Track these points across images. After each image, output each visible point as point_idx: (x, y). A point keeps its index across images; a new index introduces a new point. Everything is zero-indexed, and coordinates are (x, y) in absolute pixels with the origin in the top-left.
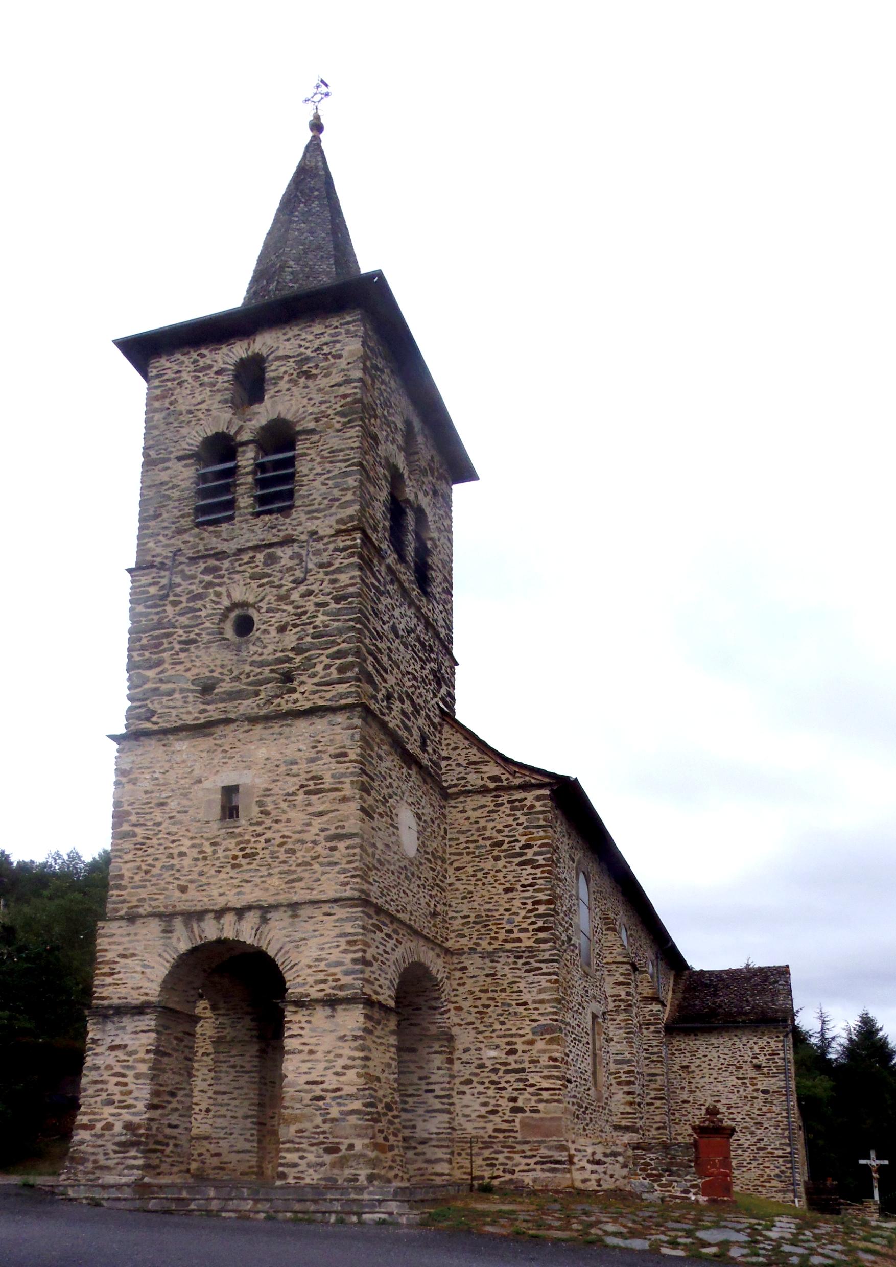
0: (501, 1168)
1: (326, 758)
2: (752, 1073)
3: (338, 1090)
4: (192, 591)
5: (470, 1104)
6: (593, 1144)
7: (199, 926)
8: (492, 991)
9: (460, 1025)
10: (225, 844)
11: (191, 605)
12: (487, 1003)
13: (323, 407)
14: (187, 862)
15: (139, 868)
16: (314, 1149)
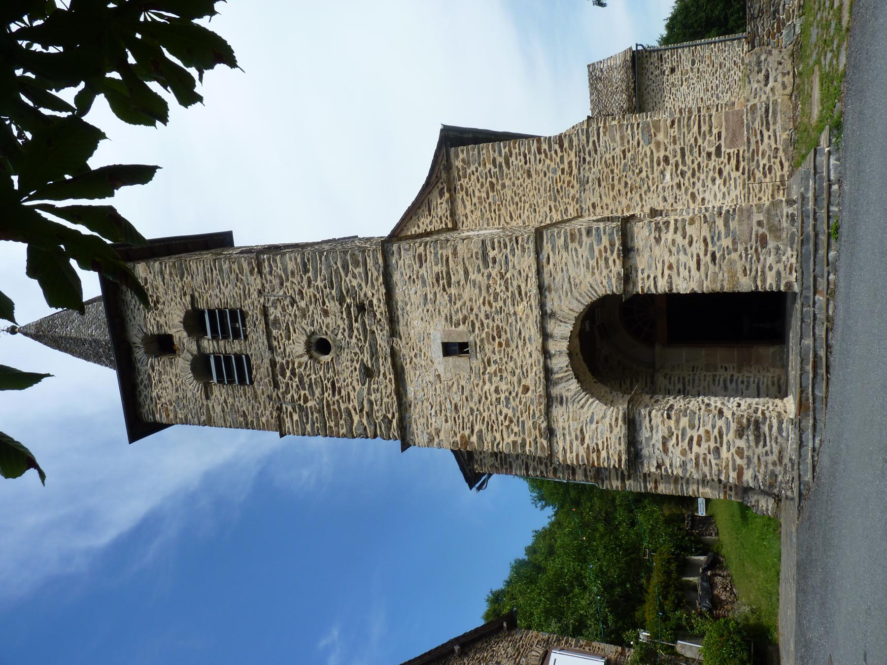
0: (772, 160)
1: (423, 271)
2: (678, 73)
3: (705, 240)
4: (297, 386)
5: (713, 193)
6: (750, 83)
7: (557, 372)
8: (613, 180)
9: (643, 206)
10: (489, 354)
11: (307, 387)
12: (623, 184)
13: (177, 290)
14: (503, 386)
15: (508, 427)
16: (762, 258)
